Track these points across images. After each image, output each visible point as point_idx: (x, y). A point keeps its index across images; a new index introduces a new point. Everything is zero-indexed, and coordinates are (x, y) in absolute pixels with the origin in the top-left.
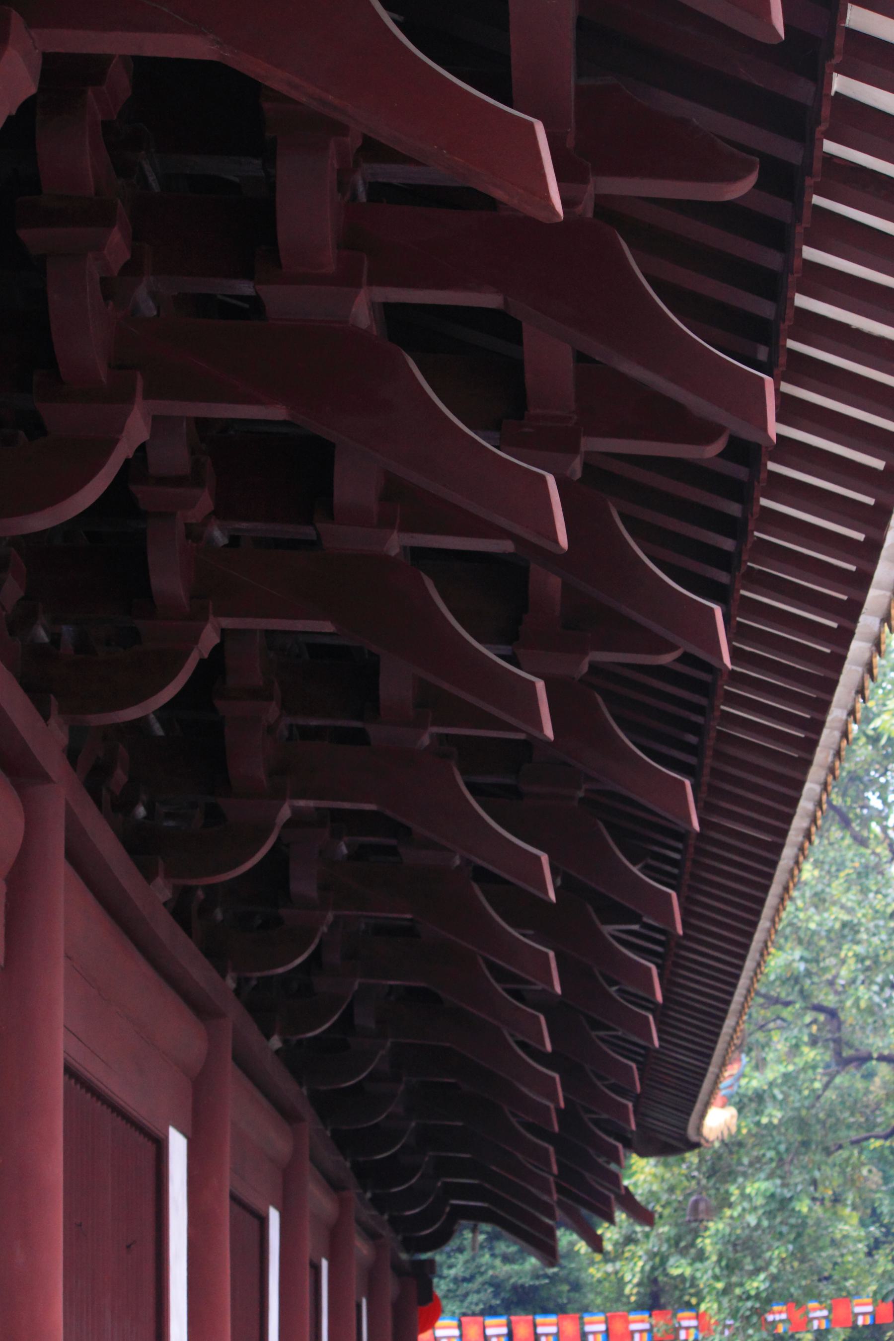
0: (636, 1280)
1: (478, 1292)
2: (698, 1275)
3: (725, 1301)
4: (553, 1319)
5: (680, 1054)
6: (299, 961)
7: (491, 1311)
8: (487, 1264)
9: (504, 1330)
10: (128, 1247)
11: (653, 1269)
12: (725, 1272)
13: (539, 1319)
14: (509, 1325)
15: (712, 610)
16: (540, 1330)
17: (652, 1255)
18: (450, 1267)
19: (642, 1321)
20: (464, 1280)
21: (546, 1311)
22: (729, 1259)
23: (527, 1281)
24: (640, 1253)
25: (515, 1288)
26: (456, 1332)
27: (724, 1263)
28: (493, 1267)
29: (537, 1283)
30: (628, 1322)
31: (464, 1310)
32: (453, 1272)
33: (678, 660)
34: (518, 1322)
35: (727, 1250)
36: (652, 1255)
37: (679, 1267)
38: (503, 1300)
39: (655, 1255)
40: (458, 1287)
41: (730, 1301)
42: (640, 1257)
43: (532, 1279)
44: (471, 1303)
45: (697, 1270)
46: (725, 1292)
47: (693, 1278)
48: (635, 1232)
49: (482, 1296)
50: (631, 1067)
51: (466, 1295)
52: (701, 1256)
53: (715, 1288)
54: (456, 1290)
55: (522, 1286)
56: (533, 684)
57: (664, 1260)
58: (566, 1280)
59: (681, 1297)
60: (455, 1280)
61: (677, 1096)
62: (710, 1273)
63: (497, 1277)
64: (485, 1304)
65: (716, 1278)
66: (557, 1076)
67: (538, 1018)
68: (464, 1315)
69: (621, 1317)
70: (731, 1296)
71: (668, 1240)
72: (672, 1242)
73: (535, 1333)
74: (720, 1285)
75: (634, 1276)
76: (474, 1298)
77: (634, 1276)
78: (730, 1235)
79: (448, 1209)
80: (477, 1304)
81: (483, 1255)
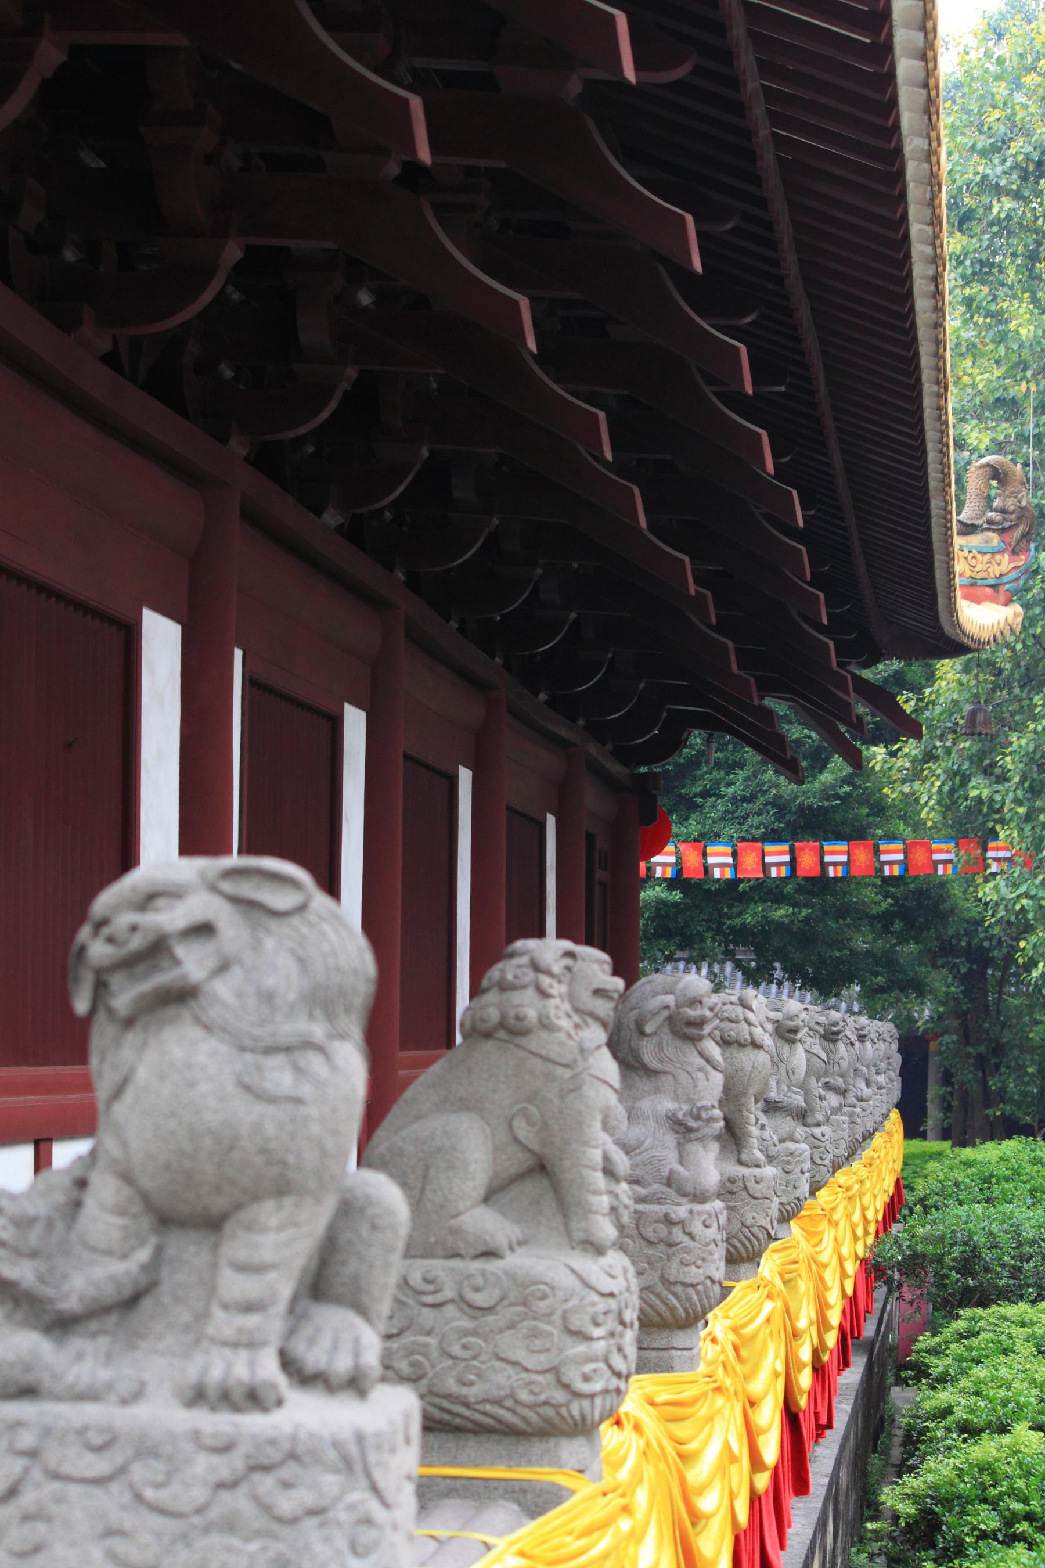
0: (932, 803)
1: (759, 813)
2: (998, 797)
3: (1028, 828)
4: (843, 846)
5: (881, 533)
6: (324, 415)
7: (773, 836)
8: (770, 781)
9: (786, 858)
10: (69, 746)
11: (953, 791)
12: (1029, 796)
13: (827, 847)
14: (792, 852)
15: (612, 17)
16: (768, 859)
17: (952, 774)
18: (729, 784)
19: (948, 852)
20: (744, 799)
21: (839, 837)
22: (1033, 780)
23: (816, 802)
24: (939, 771)
25: (801, 808)
26: (729, 860)
27: (1026, 785)
28: (777, 786)
29: (826, 804)
30: (932, 852)
31: (743, 834)
32: (731, 790)
33: (693, 72)
34: (802, 849)
35: (1031, 769)
36: (952, 774)
37: (979, 788)
38: (788, 824)
39: (955, 774)
40: (737, 807)
41: (1033, 828)
42: (938, 776)
43: (820, 800)
44: (751, 826)
45: (997, 792)
46: (1028, 818)
47: (991, 800)
48: (935, 747)
49: (763, 818)
50: (800, 550)
51: (746, 817)
52: (1003, 778)
53: (1017, 813)
54: (735, 811)
55: (810, 807)
56: (406, 101)
57: (965, 780)
58: (864, 801)
59: (984, 823)
60: (734, 800)
61: (910, 588)
62: (1011, 795)
63: (780, 796)
64: (766, 828)
65: (1018, 802)
66: (687, 559)
67: (631, 490)
68: (743, 839)
69: (922, 845)
70: (1034, 824)
71: (970, 758)
72: (976, 759)
73: (764, 864)
74: (1021, 810)
75: (930, 798)
76: (754, 820)
77: (930, 798)
78: (1034, 752)
79: (665, 714)
80: (757, 828)
81: (765, 772)
